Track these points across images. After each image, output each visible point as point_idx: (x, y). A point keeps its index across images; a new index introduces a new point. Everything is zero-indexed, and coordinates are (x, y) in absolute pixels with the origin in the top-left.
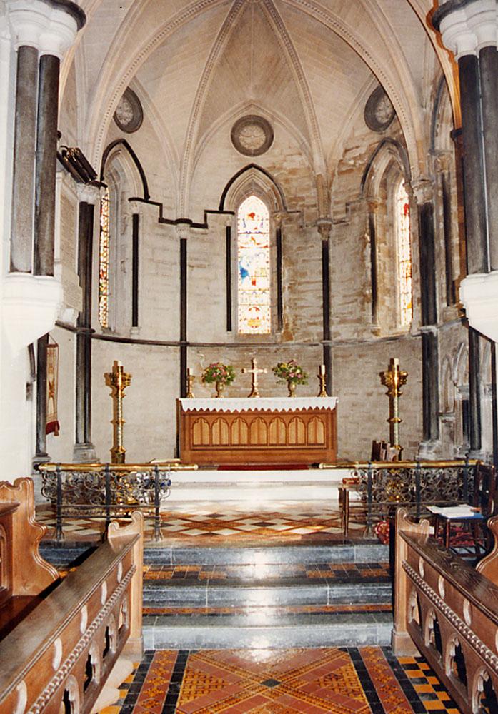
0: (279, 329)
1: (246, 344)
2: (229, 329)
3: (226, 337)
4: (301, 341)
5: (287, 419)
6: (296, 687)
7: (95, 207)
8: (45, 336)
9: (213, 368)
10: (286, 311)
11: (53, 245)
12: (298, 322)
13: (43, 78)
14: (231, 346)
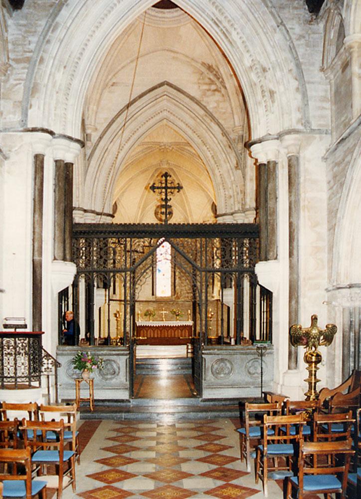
0: (174, 295)
1: (161, 302)
2: (153, 295)
3: (151, 298)
4: (183, 300)
5: (175, 329)
6: (186, 460)
7: (74, 166)
8: (64, 290)
9: (148, 311)
10: (177, 288)
11: (100, 69)
12: (182, 293)
13: (248, 89)
14: (154, 302)
